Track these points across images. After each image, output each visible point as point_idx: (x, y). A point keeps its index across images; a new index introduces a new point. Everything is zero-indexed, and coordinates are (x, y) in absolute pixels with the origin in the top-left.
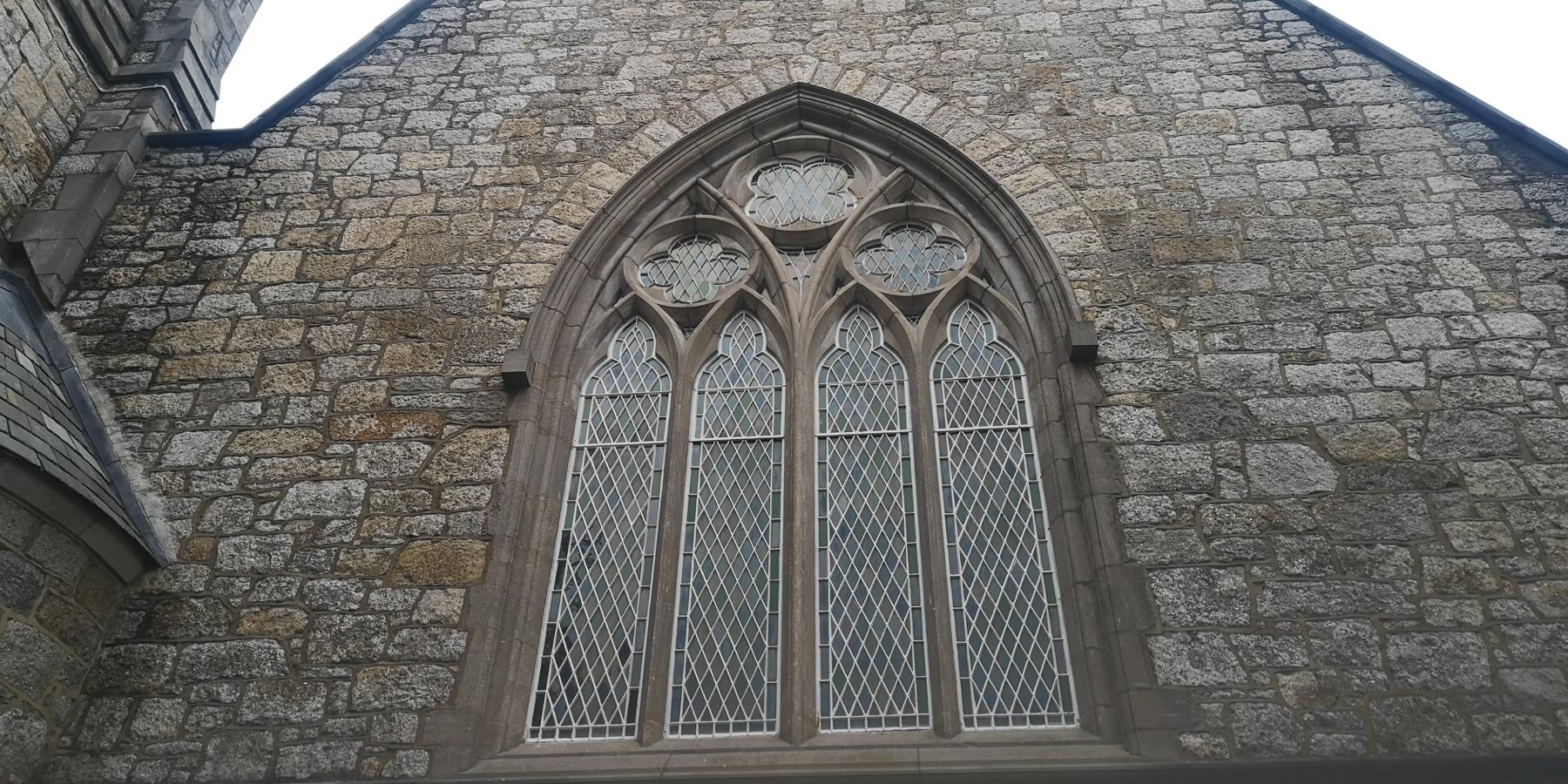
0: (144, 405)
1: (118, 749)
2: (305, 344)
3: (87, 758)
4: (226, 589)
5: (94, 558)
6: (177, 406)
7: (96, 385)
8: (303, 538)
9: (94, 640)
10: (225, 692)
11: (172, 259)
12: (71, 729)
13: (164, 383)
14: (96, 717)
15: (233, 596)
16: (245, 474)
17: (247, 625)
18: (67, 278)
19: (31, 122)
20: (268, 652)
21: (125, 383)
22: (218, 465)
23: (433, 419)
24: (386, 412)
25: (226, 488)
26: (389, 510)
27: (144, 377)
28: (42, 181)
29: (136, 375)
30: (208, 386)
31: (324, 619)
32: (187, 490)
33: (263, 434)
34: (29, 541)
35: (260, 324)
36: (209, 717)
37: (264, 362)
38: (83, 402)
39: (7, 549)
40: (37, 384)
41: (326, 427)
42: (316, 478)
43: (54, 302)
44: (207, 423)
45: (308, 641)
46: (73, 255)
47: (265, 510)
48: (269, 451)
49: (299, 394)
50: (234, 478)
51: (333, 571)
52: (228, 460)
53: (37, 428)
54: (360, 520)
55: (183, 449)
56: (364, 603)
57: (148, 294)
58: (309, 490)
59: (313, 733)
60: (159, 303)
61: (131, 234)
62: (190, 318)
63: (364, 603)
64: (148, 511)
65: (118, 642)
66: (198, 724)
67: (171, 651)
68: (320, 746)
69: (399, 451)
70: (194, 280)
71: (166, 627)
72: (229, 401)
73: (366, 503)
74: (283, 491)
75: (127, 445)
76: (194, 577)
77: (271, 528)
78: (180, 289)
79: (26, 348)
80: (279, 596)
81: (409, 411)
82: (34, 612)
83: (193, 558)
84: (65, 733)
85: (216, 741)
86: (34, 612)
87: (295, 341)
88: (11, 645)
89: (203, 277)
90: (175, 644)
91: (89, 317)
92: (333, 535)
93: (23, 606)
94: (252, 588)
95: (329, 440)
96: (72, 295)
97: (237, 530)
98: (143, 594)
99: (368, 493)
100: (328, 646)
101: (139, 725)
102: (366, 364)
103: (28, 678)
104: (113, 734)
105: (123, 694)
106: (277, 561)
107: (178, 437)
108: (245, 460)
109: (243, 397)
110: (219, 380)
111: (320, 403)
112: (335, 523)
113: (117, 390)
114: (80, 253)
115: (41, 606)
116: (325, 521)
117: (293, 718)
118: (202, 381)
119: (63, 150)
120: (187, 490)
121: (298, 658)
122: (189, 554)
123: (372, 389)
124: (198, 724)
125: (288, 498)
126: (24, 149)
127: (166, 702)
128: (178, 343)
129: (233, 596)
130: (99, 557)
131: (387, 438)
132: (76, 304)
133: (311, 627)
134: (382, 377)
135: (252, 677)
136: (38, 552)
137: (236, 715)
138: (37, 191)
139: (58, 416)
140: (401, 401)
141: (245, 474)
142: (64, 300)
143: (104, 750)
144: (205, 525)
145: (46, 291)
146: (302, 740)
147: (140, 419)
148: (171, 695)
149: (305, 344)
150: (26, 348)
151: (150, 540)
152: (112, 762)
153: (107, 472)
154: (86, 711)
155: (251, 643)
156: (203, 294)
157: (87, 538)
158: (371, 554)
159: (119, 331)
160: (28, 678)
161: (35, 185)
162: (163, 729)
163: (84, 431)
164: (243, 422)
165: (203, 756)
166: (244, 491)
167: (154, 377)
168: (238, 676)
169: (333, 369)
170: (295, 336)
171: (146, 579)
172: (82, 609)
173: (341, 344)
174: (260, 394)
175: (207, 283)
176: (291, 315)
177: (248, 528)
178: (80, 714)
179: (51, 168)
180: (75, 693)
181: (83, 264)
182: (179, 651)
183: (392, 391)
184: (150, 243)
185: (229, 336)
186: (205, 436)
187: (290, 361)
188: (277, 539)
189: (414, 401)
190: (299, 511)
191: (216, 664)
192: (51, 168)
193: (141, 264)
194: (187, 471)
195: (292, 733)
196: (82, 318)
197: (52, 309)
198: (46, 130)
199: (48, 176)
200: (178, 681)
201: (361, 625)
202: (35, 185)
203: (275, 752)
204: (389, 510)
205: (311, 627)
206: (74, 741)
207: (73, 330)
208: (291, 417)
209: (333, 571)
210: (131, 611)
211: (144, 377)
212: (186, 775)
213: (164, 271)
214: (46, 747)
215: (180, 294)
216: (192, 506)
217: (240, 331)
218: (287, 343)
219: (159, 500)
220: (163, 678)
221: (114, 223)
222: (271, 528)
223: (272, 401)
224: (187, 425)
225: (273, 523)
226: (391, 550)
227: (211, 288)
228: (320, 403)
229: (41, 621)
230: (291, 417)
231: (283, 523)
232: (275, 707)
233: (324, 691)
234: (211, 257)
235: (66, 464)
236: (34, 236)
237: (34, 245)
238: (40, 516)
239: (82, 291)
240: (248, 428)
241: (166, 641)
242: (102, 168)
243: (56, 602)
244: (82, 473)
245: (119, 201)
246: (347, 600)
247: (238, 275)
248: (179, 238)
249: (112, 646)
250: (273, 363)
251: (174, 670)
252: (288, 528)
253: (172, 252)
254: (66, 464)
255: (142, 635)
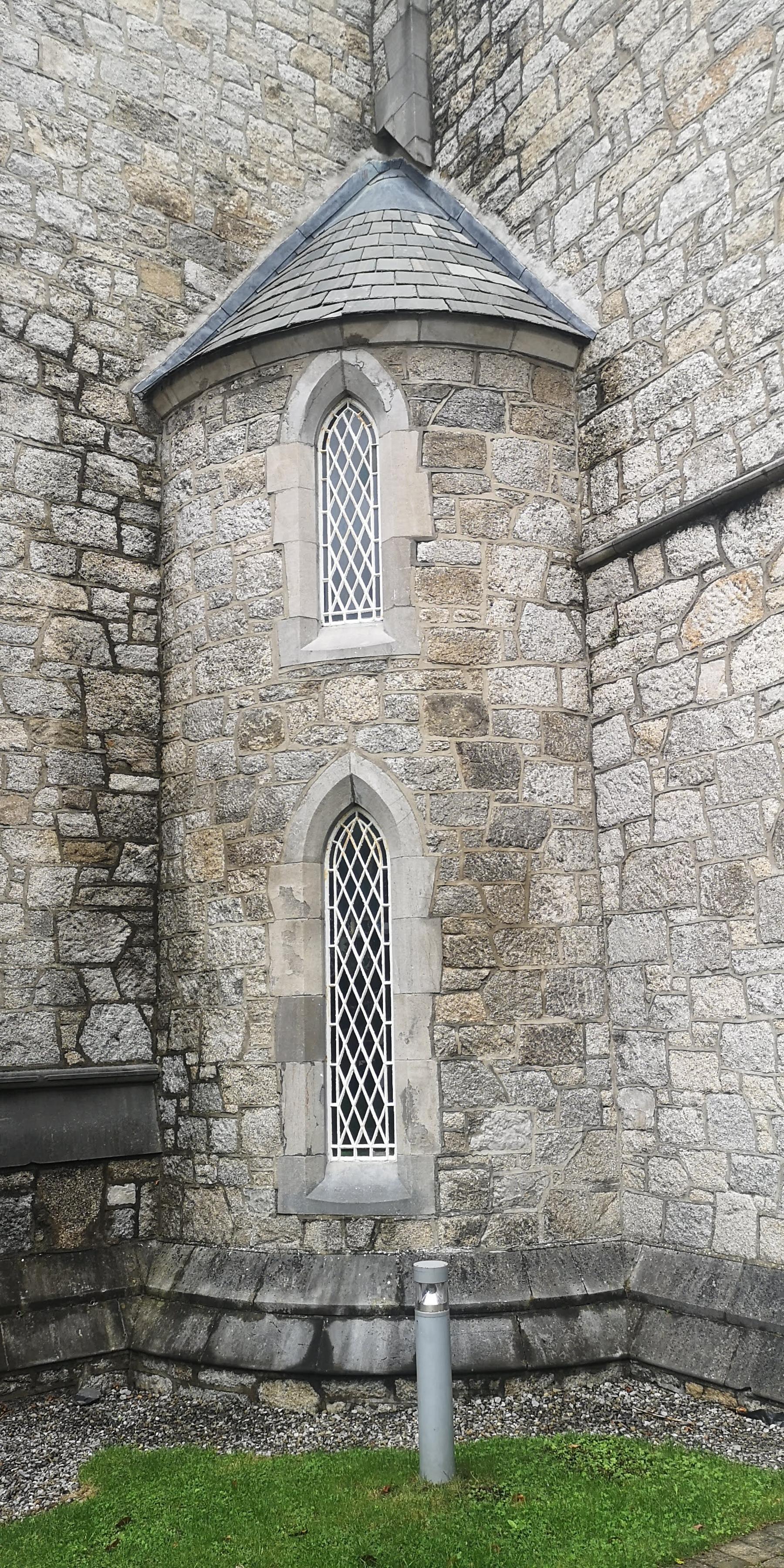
0: (521, 208)
1: (622, 502)
2: (621, 48)
3: (604, 518)
4: (646, 329)
5: (535, 361)
6: (546, 189)
7: (485, 214)
8: (689, 243)
9: (569, 426)
10: (679, 418)
11: (488, 52)
12: (585, 502)
13: (529, 175)
14: (597, 486)
15: (654, 332)
16: (621, 214)
17: (674, 352)
18: (426, 135)
19: (333, 13)
20: (699, 367)
21: (502, 197)
22: (598, 221)
23: (761, 36)
24: (718, 59)
25: (612, 238)
26: (754, 166)
27: (513, 181)
28: (372, 60)
29: (506, 184)
30: (561, 153)
31: (734, 310)
32: (583, 261)
33: (620, 166)
34: (475, 374)
35: (576, 58)
36: (676, 445)
37: (595, 92)
38: (482, 235)
39: (462, 388)
40: (439, 243)
41: (667, 121)
42: (678, 178)
43: (428, 162)
44: (574, 188)
45: (728, 337)
46: (420, 108)
47: (649, 238)
48: (631, 179)
49: (634, 104)
50: (613, 224)
51: (726, 259)
52: (603, 212)
53: (443, 279)
54: (731, 194)
55: (568, 224)
56: (765, 273)
57: (484, 102)
58: (677, 192)
59: (763, 416)
60: (496, 103)
61: (450, 54)
62: (523, 98)
63: (765, 273)
64: (563, 299)
65: (588, 419)
66: (669, 454)
67: (626, 405)
68: (772, 425)
69: (741, 97)
70: (511, 58)
71: (615, 388)
72: (581, 154)
73: (731, 172)
74: (656, 209)
75: (527, 250)
76: (618, 335)
77: (660, 251)
78: (505, 76)
79: (422, 217)
80: (689, 311)
81: (737, 43)
82: (508, 426)
83: (612, 318)
84: (582, 506)
85: (688, 462)
86: (508, 426)
87: (610, 52)
88: (504, 459)
89: (516, 49)
90: (627, 398)
91: (457, 156)
92: (713, 224)
93: (498, 425)
94: (666, 316)
95: (676, 131)
96: (437, 146)
97: (635, 270)
98: (589, 370)
99: (730, 161)
100: (747, 332)
101: (628, 477)
102: (679, 26)
103: (530, 477)
104: (614, 492)
105: (608, 458)
106: (676, 279)
107: (558, 217)
108: (615, 201)
109: (592, 143)
110: (567, 140)
111: (654, 100)
112: (710, 212)
113: (501, 207)
114: (424, 103)
115: (511, 420)
116: (700, 217)
117: (741, 413)
118: (554, 151)
119: (372, 18)
120: (583, 261)
121: (726, 358)
122: (609, 319)
123: (694, 49)
124: (669, 454)
125: (663, 213)
126: (341, 42)
127: (639, 449)
128: (524, 130)
129: (654, 332)
130: (537, 358)
131: (725, 92)
132: (443, 152)
133: (726, 324)
134: (698, 29)
135: (695, 394)
136: (486, 378)
137: (695, 433)
138: (373, 71)
139: (462, 258)
140: (725, 40)
141: (621, 214)
142: (434, 156)
143: (613, 507)
144: (610, 283)
145: (416, 158)
146: (758, 427)
147: (525, 221)
148: (641, 441)
149: (621, 48)
150: (422, 217)
151: (575, 322)
152: (620, 513)
153: (522, 284)
154: (589, 483)
155: (682, 366)
156: (522, 66)
157: (518, 347)
158: (753, 221)
159: (479, 153)
160: (530, 477)
161: (368, 68)
162: (647, 471)
163: (493, 260)
164: (600, 166)
165: (685, 480)
166: (628, 232)
167: (520, 176)
168: (684, 399)
169: (651, 58)
170: (608, 48)
171: (585, 355)
172: (546, 407)
173: (649, 23)
174: (603, 129)
175: (520, 52)
176: (596, 28)
177: (643, 263)
178: (586, 487)
179: (371, 43)
180: (575, 473)
181: (432, 112)
182: (632, 402)
183: (713, 35)
184: (467, 51)
185: (557, 91)
186: (576, 201)
187: (613, 76)
188: (668, 258)
189: (736, 31)
190: (677, 220)
191: (663, 399)
192: (371, 43)
193: (469, 77)
194: (576, 244)
195: (744, 427)
196: (451, 163)
197: (429, 169)
198: (348, 11)
199: (373, 52)
200: (642, 427)
201: (768, 296)
202: (368, 68)
203: (738, 449)
204: (754, 166)
205: (726, 324)
206: (591, 509)
207: (451, 177)
208: (636, 132)
209: (726, 259)
210: (585, 389)
211: (513, 181)
212: (677, 499)
213: (487, 71)
214: (573, 523)
215: (506, 81)
216: (593, 271)
217: (564, 78)
218: (604, 60)
219: (567, 283)
220: (630, 431)
221: (436, 54)
222: (660, 251)
223: (614, 129)
224: (560, 201)
225: (660, 246)
226: (770, 205)
227: (526, 55)
228: (654, 100)
229: (517, 431)
230: (636, 132)
231: (668, 240)
232: (724, 411)
233: (757, 374)
234: (515, 24)
235: (476, 296)
236: (388, 115)
237: (391, 123)
238: (474, 350)
239: (441, 138)
240: (608, 168)
241: (620, 399)
242: (402, 11)
243: (521, 410)
244: (494, 293)
245: (430, 29)
246: (747, 279)
247: (541, 25)
248: (483, 27)
249: (585, 424)
250: (601, 89)
251: (635, 423)
252: (673, 242)
253: (485, 46)
254: (476, 296)
255: (602, 403)
